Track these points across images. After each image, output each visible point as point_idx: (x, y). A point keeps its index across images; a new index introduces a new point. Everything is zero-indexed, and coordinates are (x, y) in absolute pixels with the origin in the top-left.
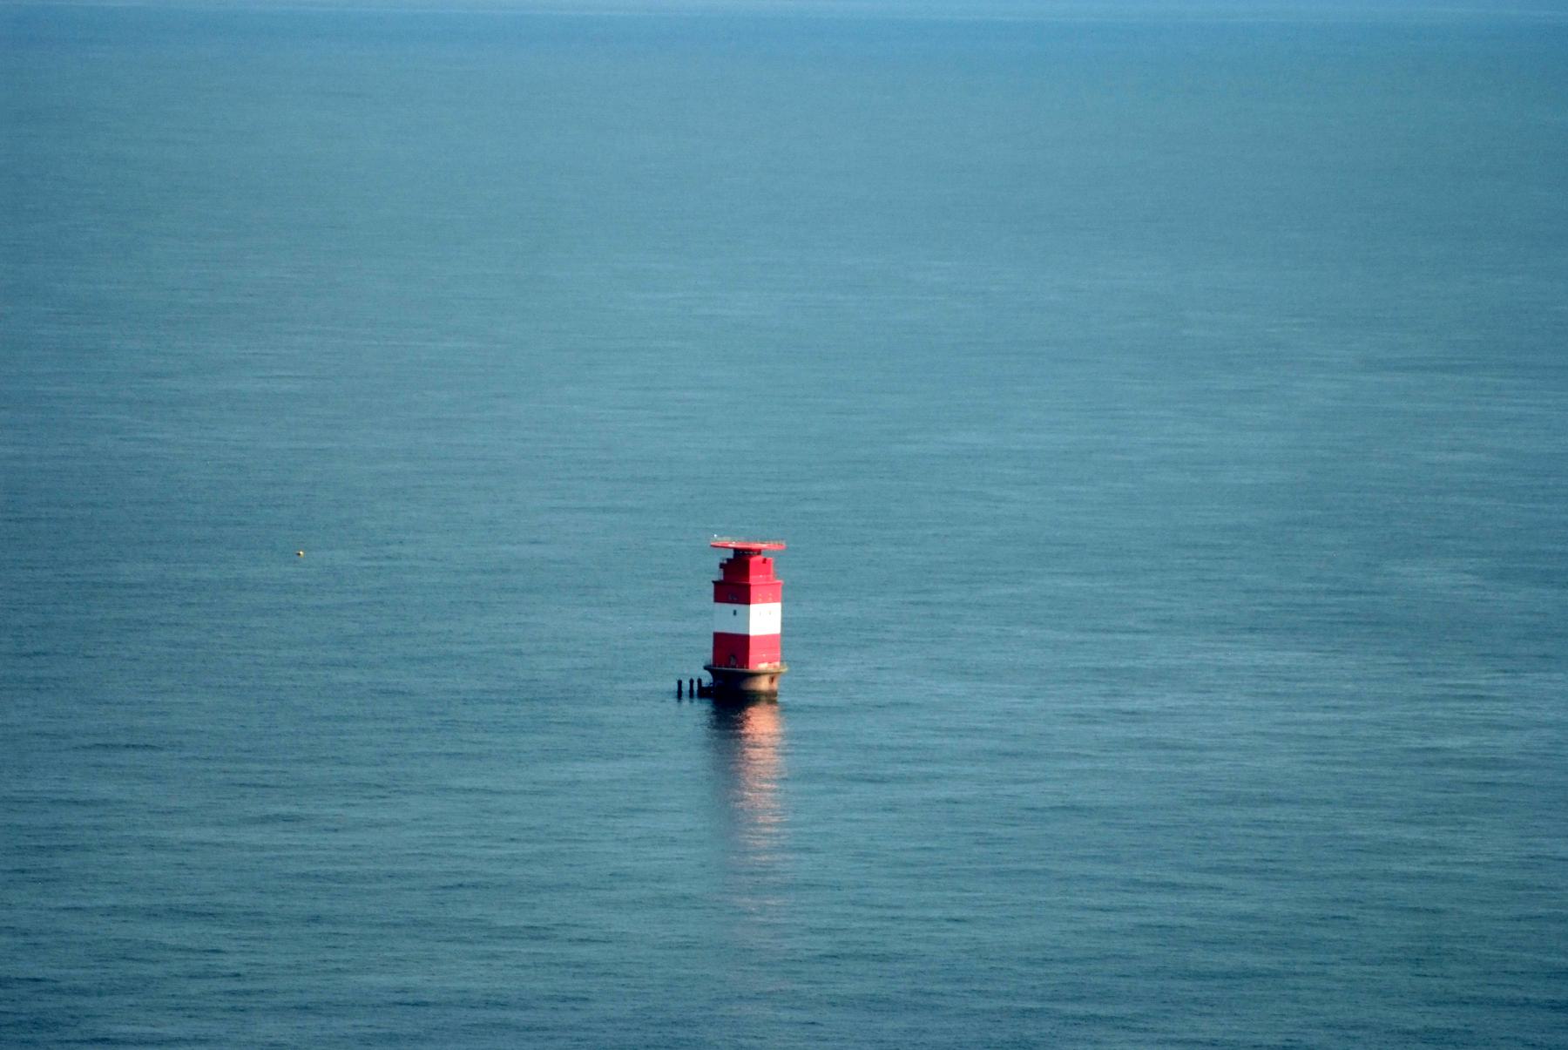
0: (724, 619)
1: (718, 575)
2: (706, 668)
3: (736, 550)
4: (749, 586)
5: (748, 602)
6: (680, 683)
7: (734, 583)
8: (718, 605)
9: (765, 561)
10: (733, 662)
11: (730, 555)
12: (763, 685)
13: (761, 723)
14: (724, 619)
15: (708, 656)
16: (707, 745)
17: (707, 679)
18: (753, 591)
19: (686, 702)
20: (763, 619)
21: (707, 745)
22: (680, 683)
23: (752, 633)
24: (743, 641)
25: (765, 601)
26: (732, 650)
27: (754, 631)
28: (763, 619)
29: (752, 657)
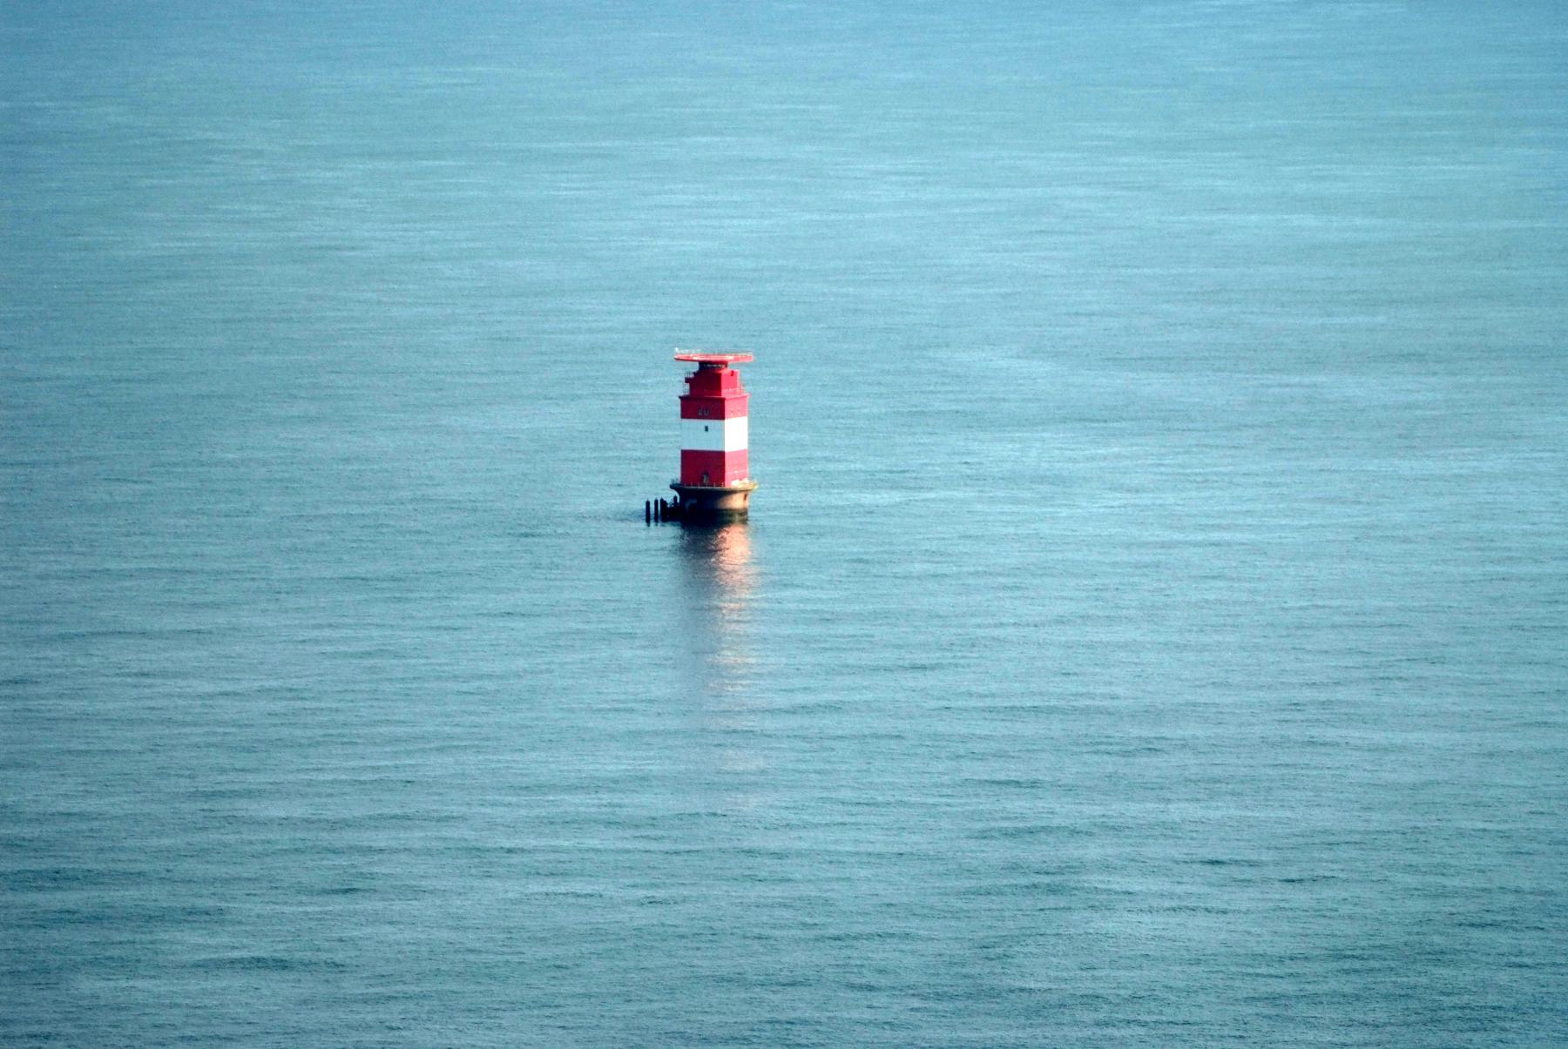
0: (697, 435)
1: (684, 389)
2: (672, 487)
3: (702, 363)
4: (723, 400)
5: (722, 417)
6: (648, 504)
7: (705, 393)
8: (686, 421)
9: (733, 373)
10: (705, 480)
11: (696, 367)
12: (736, 502)
13: (736, 545)
14: (697, 435)
15: (676, 474)
16: (673, 552)
17: (670, 496)
18: (728, 407)
19: (652, 524)
20: (733, 434)
21: (673, 552)
22: (648, 504)
23: (727, 450)
24: (719, 457)
25: (736, 416)
26: (703, 470)
27: (729, 447)
28: (733, 434)
29: (728, 474)
